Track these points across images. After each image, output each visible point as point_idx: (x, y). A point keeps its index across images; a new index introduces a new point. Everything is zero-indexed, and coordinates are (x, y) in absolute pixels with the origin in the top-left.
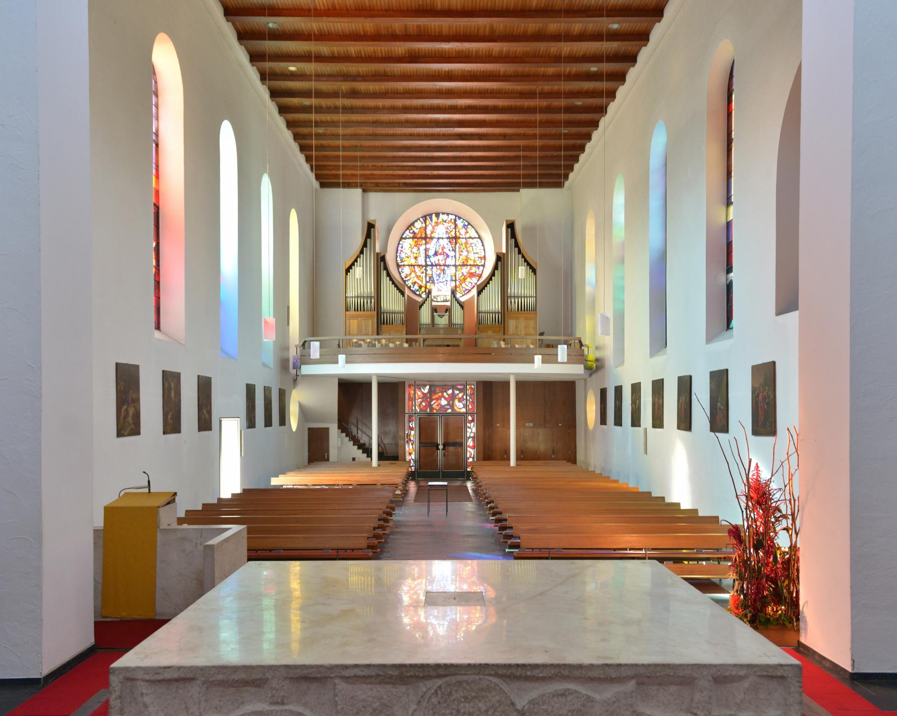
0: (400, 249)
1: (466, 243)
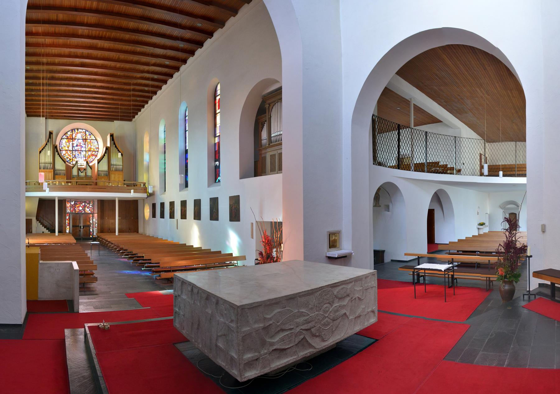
0: (61, 143)
1: (90, 142)
